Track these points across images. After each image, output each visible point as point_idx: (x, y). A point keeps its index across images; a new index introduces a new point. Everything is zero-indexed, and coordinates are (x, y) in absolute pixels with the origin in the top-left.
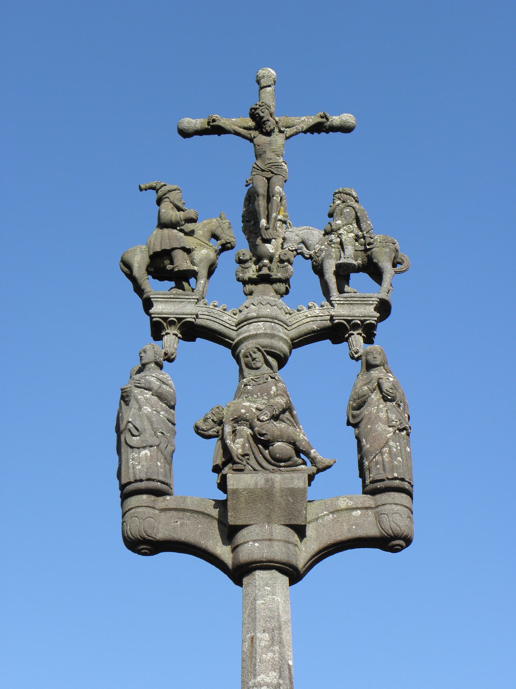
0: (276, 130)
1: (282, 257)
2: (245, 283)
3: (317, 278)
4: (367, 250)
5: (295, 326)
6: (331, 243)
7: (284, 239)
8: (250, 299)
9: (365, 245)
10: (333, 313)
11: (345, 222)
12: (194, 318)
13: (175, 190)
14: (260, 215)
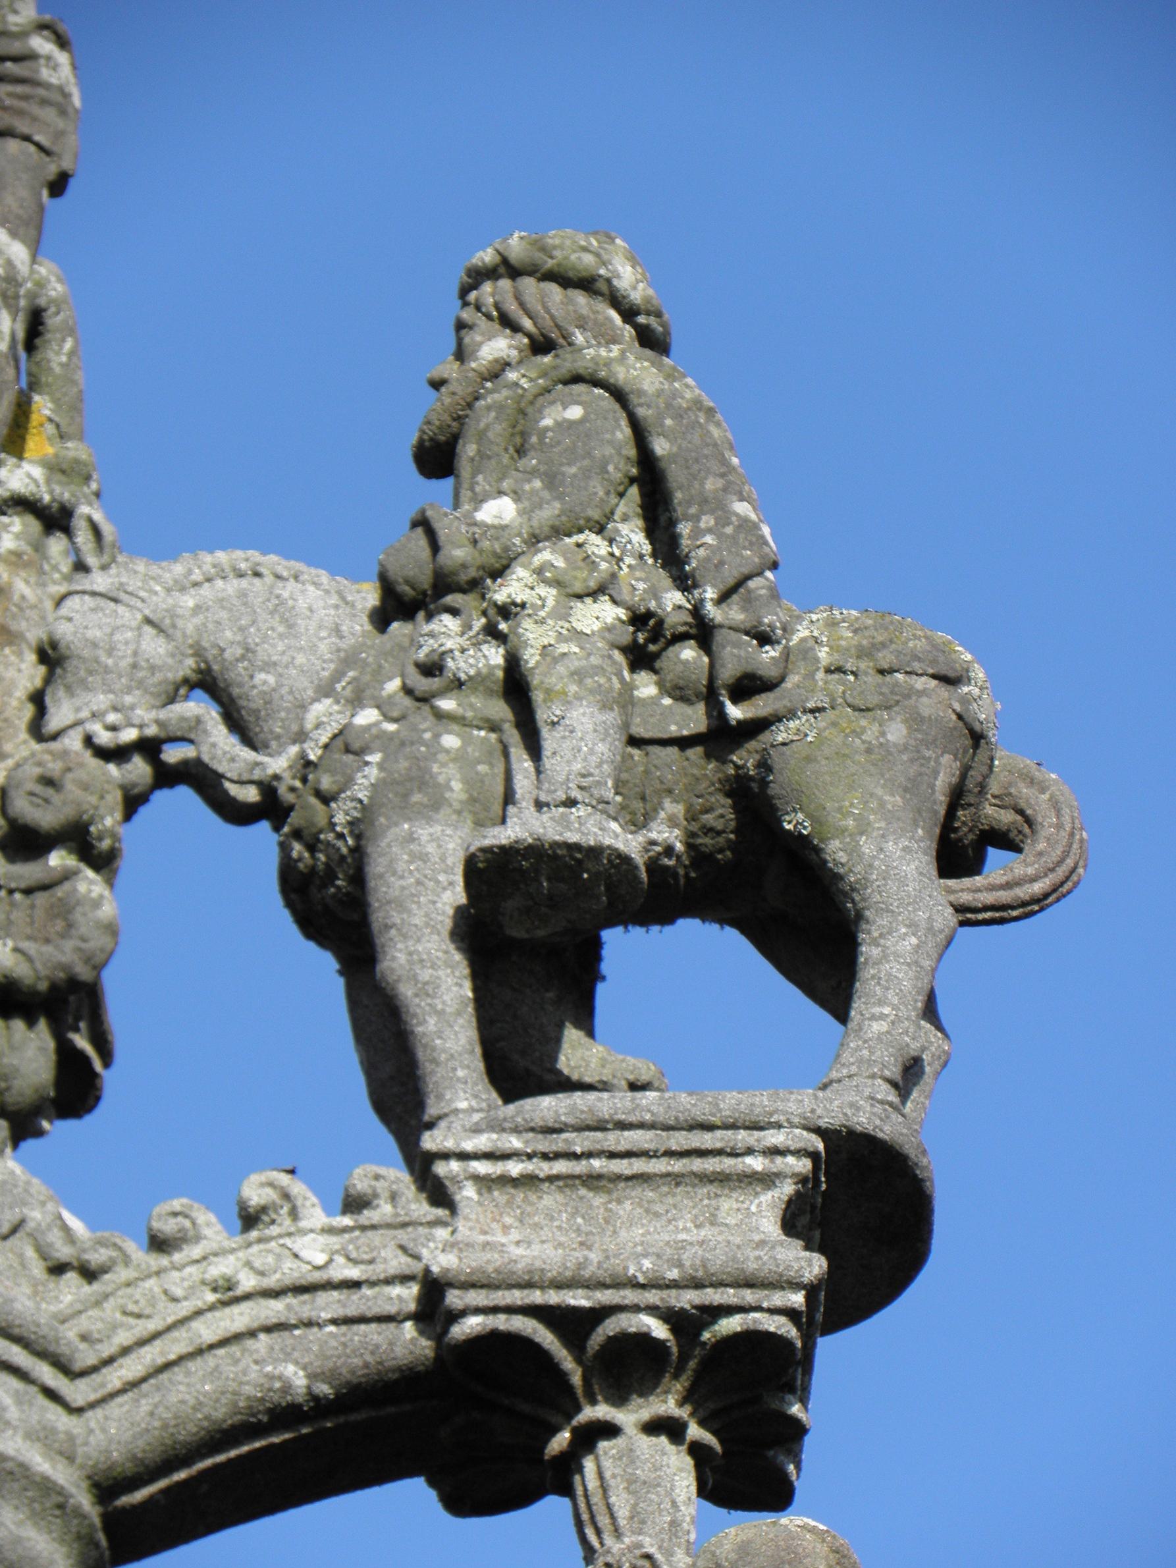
3: (321, 967)
6: (435, 683)
7: (51, 657)
10: (441, 1262)
11: (550, 512)
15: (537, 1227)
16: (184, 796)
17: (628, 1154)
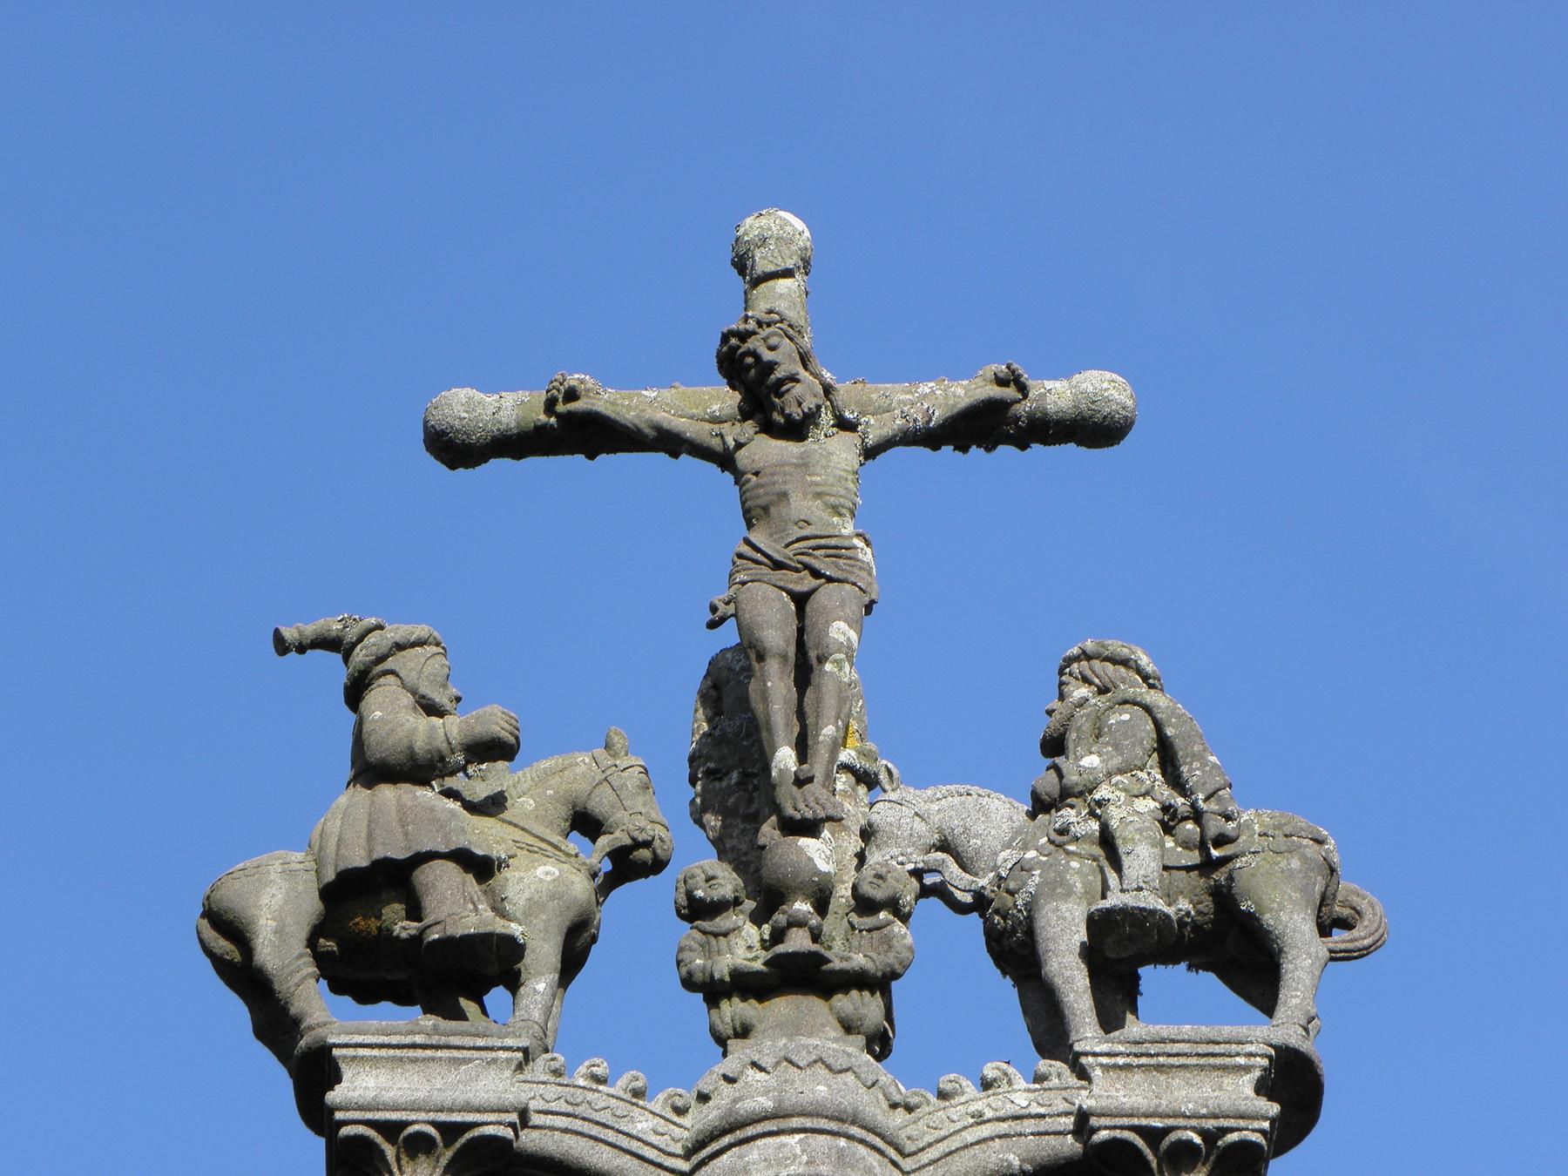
0: (826, 418)
1: (866, 889)
2: (714, 991)
3: (1005, 991)
4: (1212, 861)
5: (932, 1153)
6: (1065, 838)
7: (867, 834)
8: (740, 1050)
9: (1202, 846)
10: (1088, 1103)
11: (1116, 761)
12: (512, 1125)
13: (420, 643)
14: (769, 730)
15: (1133, 1089)
16: (934, 902)
17: (1177, 1055)
